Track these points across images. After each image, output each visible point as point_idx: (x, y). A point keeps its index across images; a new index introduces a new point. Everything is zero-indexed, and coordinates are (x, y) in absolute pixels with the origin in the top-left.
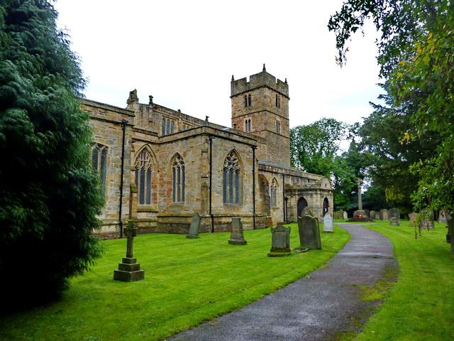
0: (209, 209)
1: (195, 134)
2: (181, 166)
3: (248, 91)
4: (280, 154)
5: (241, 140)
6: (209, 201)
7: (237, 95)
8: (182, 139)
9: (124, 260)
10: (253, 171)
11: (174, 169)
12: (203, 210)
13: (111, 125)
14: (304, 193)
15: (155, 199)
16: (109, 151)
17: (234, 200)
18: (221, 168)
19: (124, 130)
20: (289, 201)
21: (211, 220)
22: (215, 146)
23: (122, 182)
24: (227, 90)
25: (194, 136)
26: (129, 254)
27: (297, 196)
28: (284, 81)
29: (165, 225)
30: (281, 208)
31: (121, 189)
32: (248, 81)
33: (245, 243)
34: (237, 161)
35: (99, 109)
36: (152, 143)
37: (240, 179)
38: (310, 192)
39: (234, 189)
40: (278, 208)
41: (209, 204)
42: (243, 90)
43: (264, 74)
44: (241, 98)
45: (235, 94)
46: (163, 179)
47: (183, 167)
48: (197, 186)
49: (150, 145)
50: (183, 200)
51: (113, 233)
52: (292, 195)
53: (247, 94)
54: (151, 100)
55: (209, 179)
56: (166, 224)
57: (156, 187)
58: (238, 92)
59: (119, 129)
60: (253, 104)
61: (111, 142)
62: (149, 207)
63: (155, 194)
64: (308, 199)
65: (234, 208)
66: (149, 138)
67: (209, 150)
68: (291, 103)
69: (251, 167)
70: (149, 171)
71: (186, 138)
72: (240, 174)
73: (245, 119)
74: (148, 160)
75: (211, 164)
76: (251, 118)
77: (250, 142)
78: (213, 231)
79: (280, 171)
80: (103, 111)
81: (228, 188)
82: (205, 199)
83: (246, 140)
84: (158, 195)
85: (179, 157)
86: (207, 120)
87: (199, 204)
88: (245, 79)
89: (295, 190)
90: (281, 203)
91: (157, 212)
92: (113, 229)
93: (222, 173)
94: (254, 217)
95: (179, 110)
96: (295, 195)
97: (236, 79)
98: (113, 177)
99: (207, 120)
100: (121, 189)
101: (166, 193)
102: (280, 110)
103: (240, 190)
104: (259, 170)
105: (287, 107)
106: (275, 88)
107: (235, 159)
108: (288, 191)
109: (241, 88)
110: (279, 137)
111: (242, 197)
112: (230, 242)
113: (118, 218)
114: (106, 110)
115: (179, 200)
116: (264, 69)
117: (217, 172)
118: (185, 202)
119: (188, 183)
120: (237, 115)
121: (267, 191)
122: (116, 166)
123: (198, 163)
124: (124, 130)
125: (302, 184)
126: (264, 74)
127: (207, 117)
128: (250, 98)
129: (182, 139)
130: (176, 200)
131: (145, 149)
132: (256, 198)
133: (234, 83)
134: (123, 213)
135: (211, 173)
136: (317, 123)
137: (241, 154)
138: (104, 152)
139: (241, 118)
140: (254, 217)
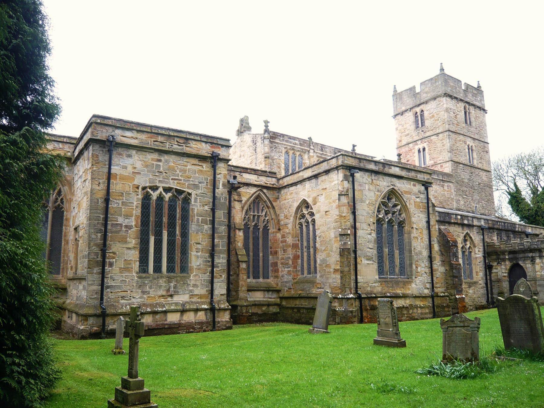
0: (353, 284)
1: (327, 168)
2: (310, 220)
3: (419, 105)
4: (476, 197)
5: (403, 173)
6: (353, 272)
7: (402, 113)
8: (309, 178)
9: (125, 384)
10: (428, 222)
11: (301, 224)
12: (343, 288)
13: (196, 161)
14: (521, 255)
15: (277, 271)
16: (193, 200)
17: (397, 270)
18: (373, 220)
19: (214, 167)
20: (494, 271)
21: (357, 303)
22: (360, 185)
23: (213, 245)
24: (51, 45)
25: (327, 172)
26: (132, 373)
27: (507, 263)
28: (476, 86)
29: (290, 311)
30: (482, 282)
31: (212, 256)
32: (418, 90)
33: (403, 344)
34: (399, 207)
35: (176, 139)
36: (268, 188)
37: (406, 236)
38: (530, 255)
39: (397, 252)
40: (476, 283)
41: (353, 277)
42: (412, 105)
43: (444, 77)
44: (409, 117)
45: (400, 111)
46: (285, 241)
47: (314, 221)
48: (334, 249)
49: (265, 191)
50: (316, 273)
51: (201, 323)
52: (500, 260)
53: (418, 110)
54: (267, 126)
55: (352, 237)
56: (293, 308)
57: (276, 253)
58: (404, 108)
59: (206, 167)
60: (427, 123)
61: (196, 187)
62: (267, 283)
63: (275, 264)
64: (527, 266)
65: (397, 283)
66: (263, 180)
67: (351, 192)
68: (488, 118)
69: (423, 217)
70: (266, 229)
71: (316, 176)
72: (406, 228)
73: (417, 148)
74: (264, 213)
75: (354, 213)
76: (425, 145)
77: (420, 177)
78: (361, 321)
79: (476, 223)
80: (181, 141)
81: (386, 250)
82: (346, 269)
83: (412, 175)
84: (280, 265)
85: (308, 206)
86: (354, 150)
87: (338, 276)
88: (414, 87)
89: (503, 253)
90: (481, 274)
91: (278, 291)
92: (201, 316)
93: (374, 227)
94: (432, 297)
95: (310, 138)
96: (504, 260)
97: (399, 90)
98: (200, 237)
99: (354, 150)
100: (212, 256)
101: (291, 262)
102: (472, 129)
103: (407, 254)
104: (438, 221)
105: (482, 127)
106: (461, 96)
107: (395, 206)
108: (491, 255)
109: (409, 102)
110: (473, 170)
111: (411, 265)
112: (376, 342)
113: (209, 300)
114: (187, 139)
115: (309, 273)
116: (442, 70)
117: (365, 226)
118: (318, 275)
119: (321, 245)
120: (404, 143)
121: (456, 255)
122: (204, 222)
123: (335, 213)
124: (214, 167)
125: (515, 242)
126: (444, 77)
127: (266, 122)
128: (422, 116)
129: (309, 178)
130: (306, 271)
131: (258, 197)
132: (435, 267)
133: (397, 96)
134: (217, 292)
135: (355, 227)
136: (483, 96)
137: (405, 197)
138: (187, 200)
139: (411, 145)
140: (432, 297)
